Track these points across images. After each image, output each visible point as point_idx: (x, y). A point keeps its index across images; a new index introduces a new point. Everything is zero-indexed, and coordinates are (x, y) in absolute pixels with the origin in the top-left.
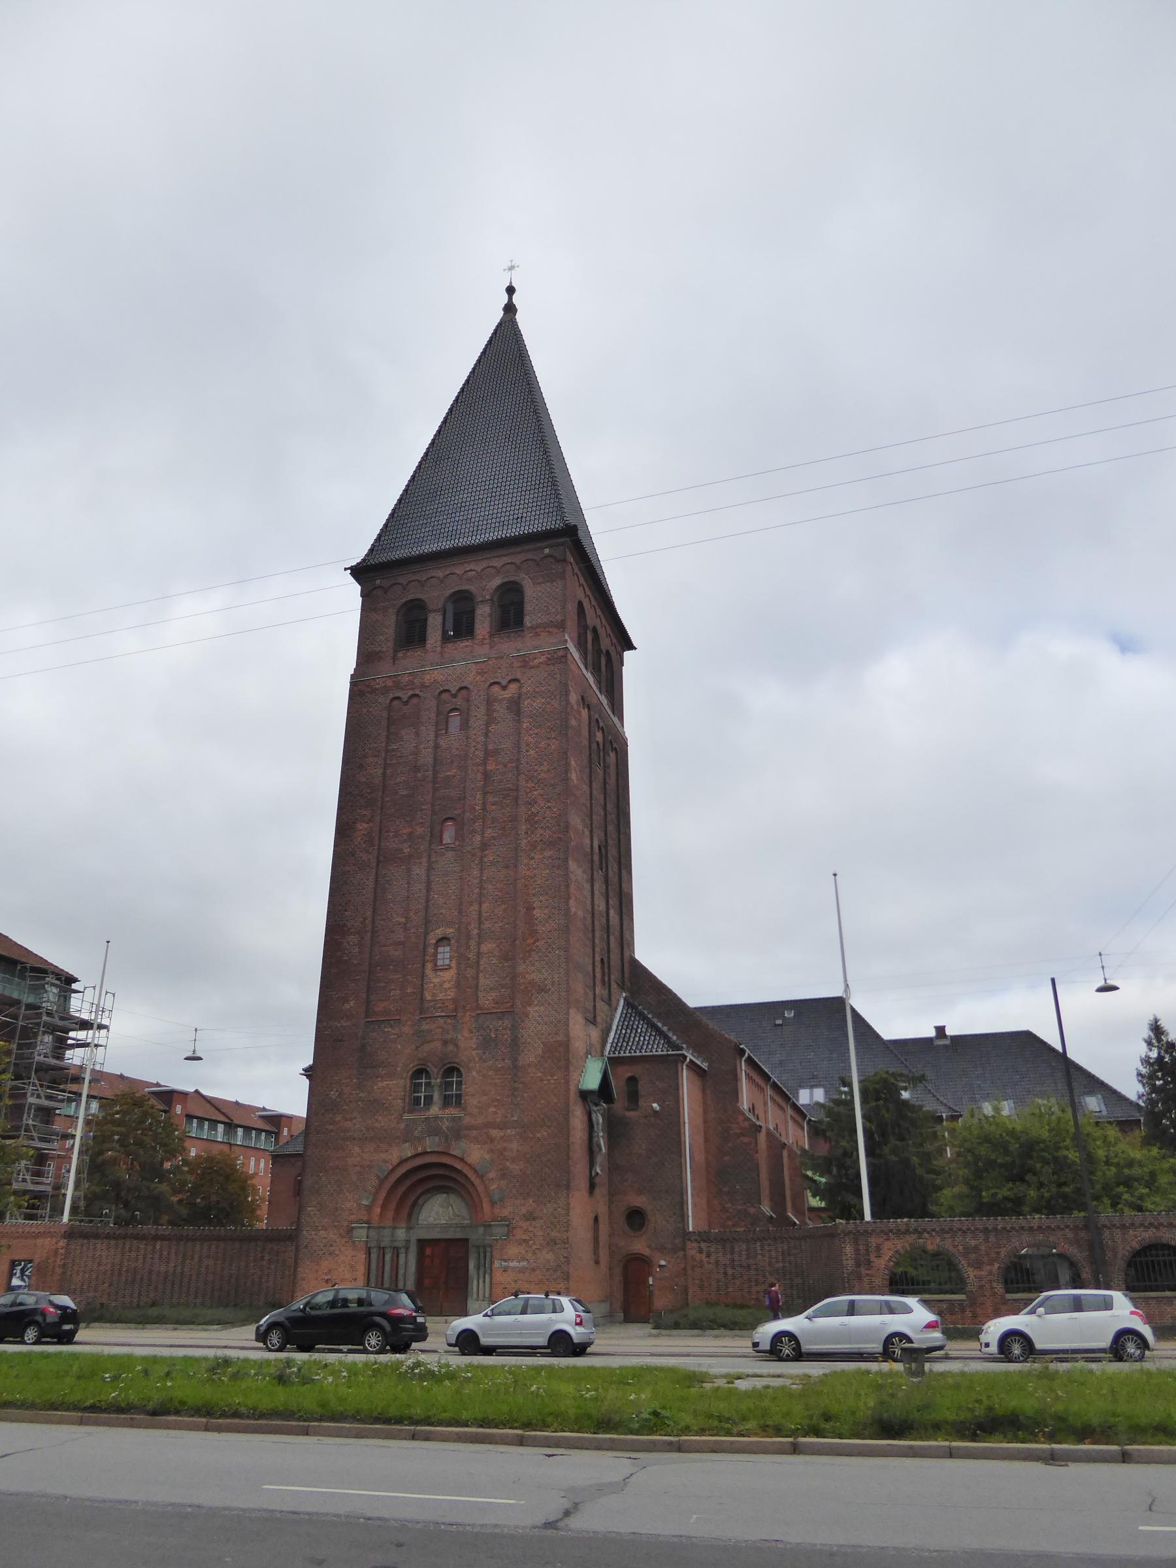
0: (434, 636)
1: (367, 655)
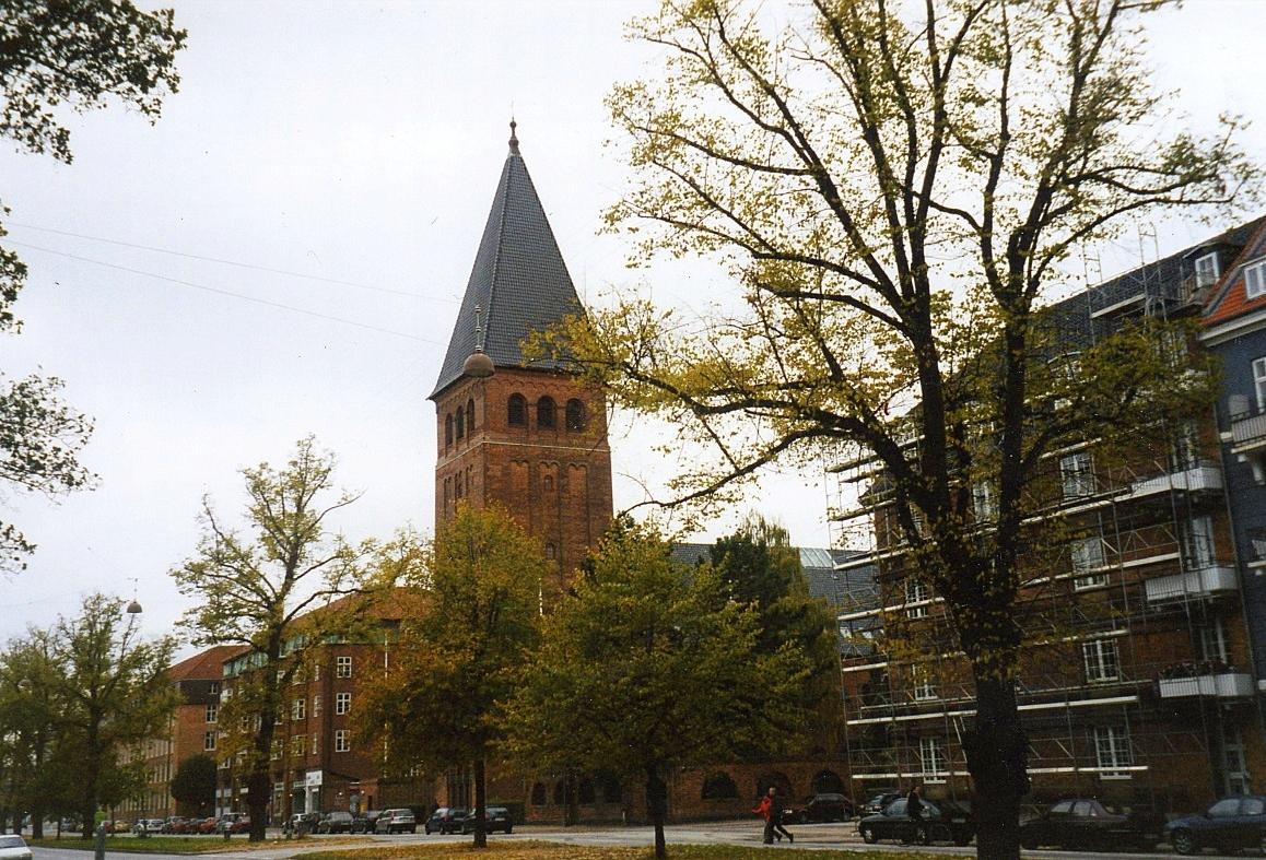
0: (465, 433)
1: (440, 455)
